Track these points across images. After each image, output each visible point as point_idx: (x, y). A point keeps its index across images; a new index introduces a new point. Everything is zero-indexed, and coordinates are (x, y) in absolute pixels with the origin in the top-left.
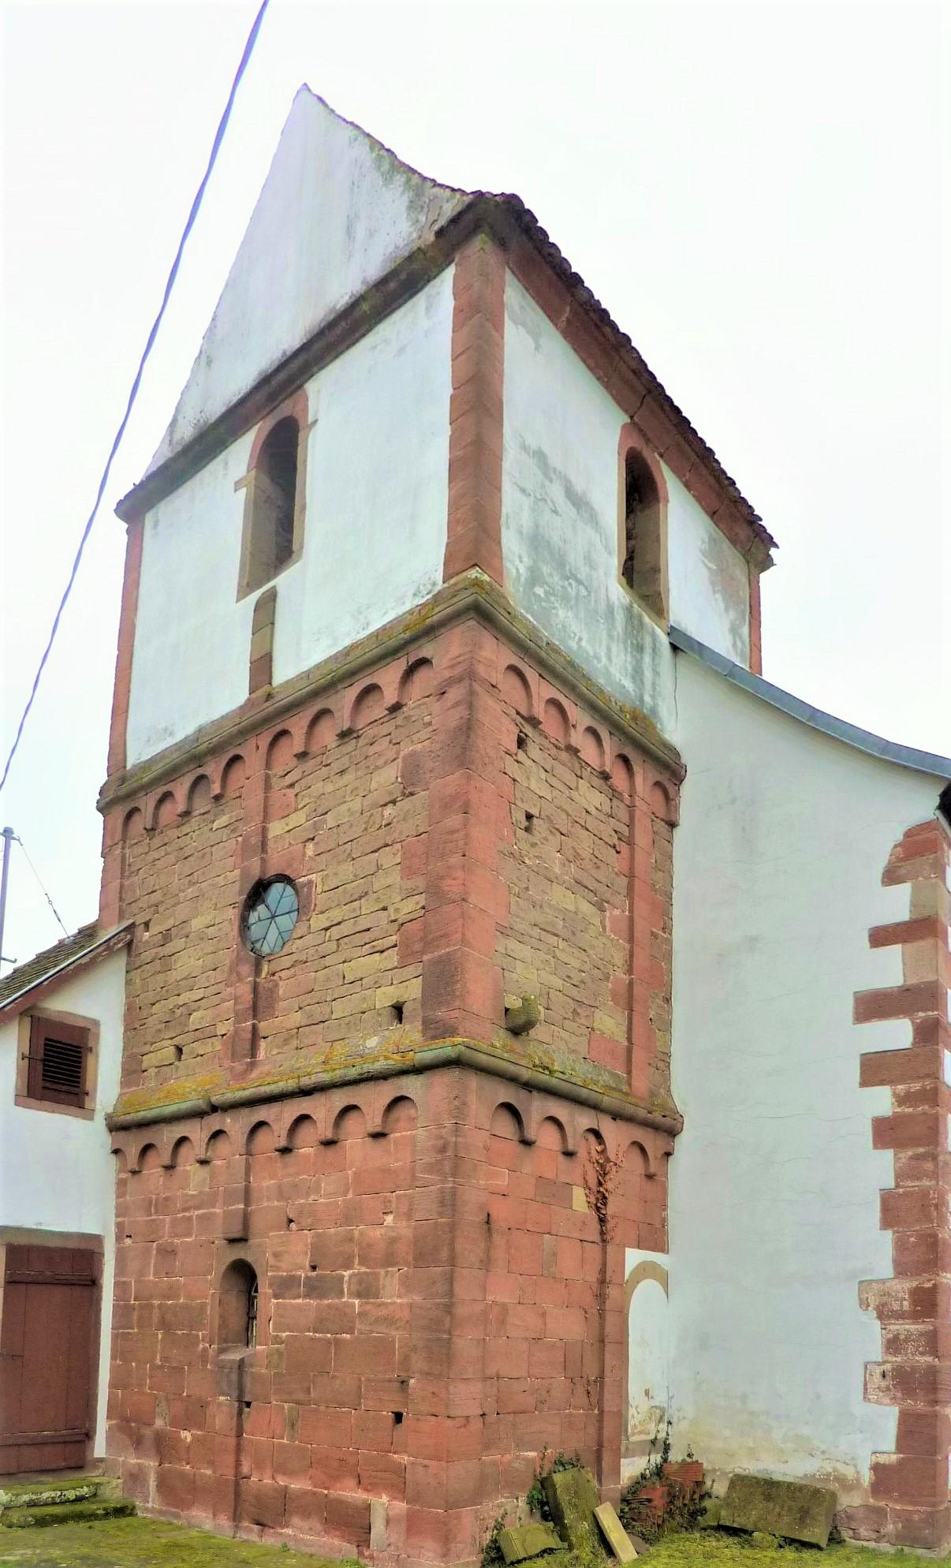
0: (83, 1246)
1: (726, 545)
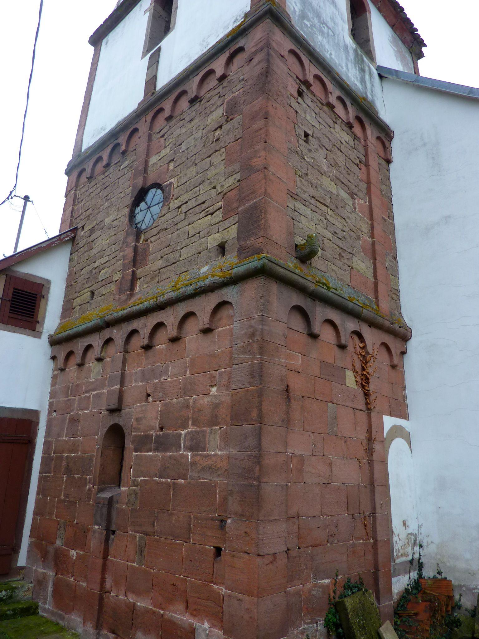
0: (25, 417)
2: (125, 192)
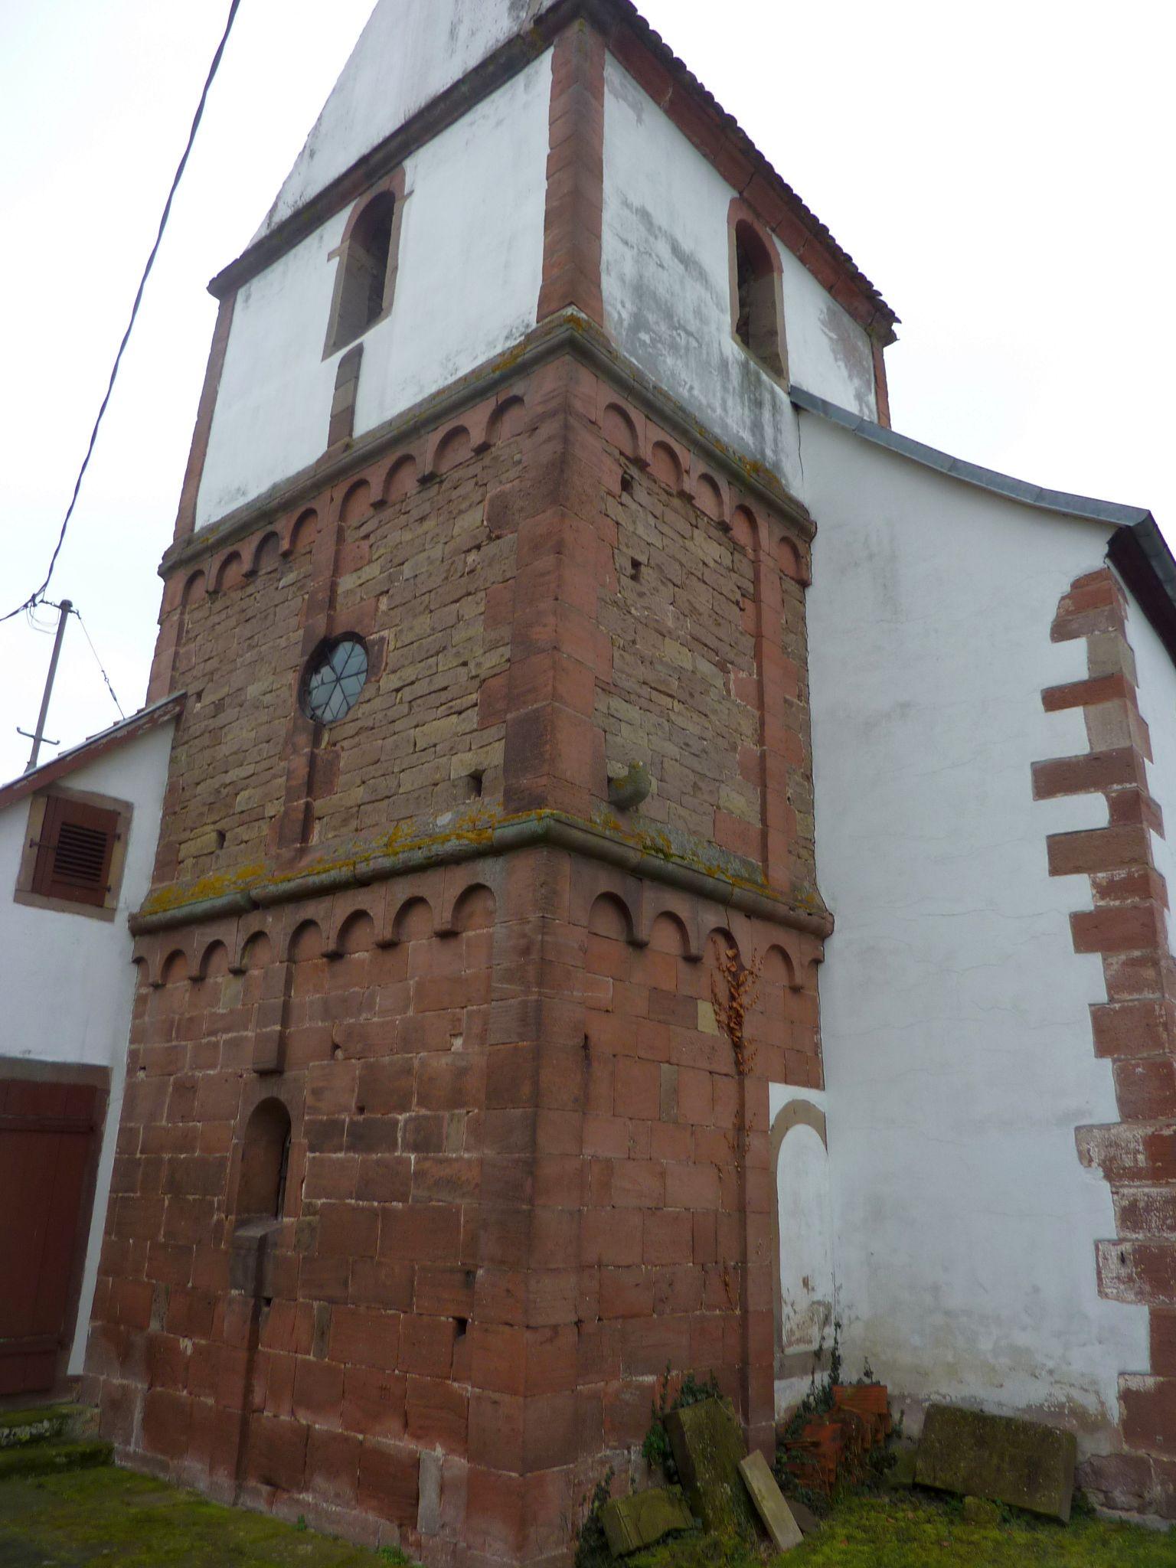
1: (846, 319)
2: (289, 640)
